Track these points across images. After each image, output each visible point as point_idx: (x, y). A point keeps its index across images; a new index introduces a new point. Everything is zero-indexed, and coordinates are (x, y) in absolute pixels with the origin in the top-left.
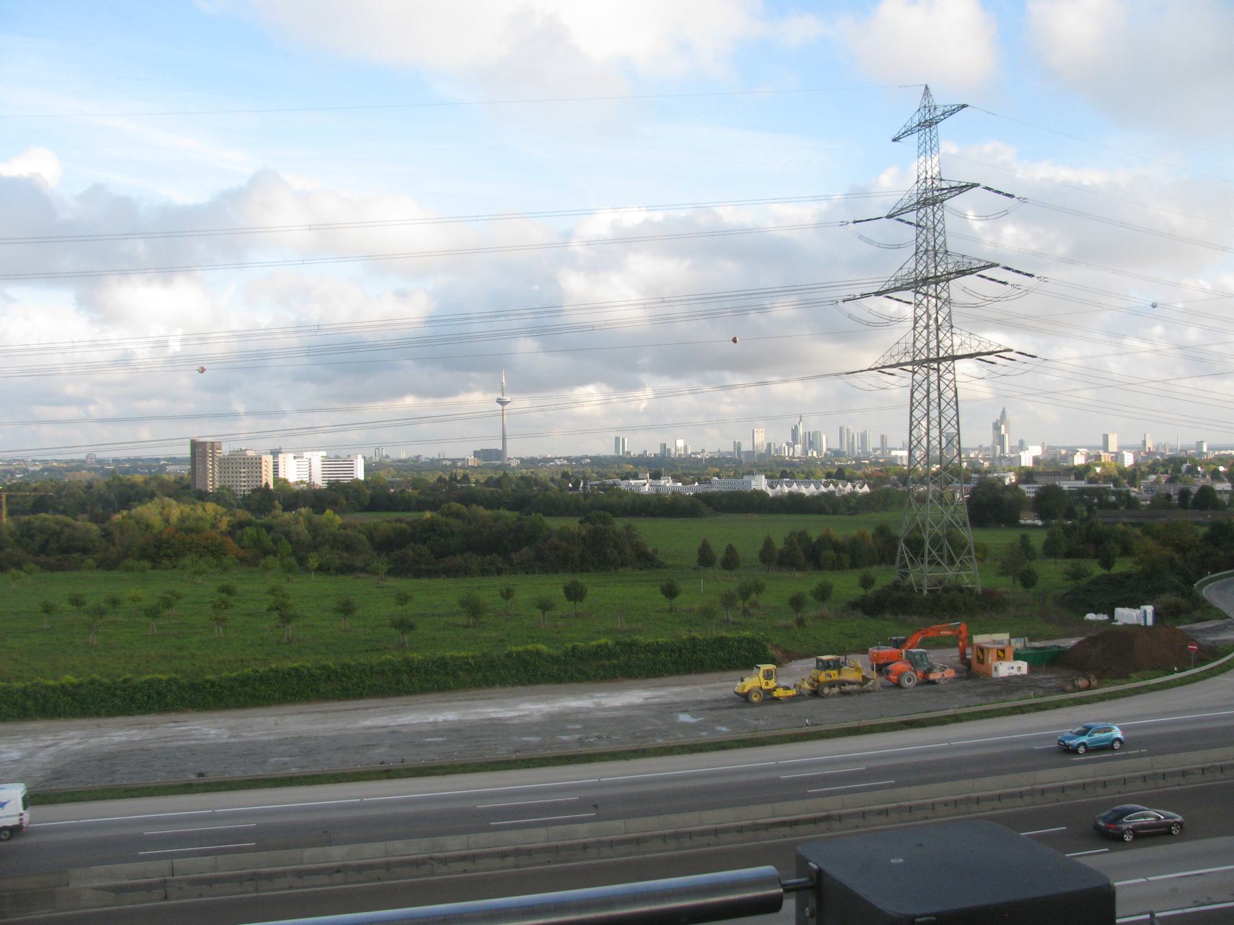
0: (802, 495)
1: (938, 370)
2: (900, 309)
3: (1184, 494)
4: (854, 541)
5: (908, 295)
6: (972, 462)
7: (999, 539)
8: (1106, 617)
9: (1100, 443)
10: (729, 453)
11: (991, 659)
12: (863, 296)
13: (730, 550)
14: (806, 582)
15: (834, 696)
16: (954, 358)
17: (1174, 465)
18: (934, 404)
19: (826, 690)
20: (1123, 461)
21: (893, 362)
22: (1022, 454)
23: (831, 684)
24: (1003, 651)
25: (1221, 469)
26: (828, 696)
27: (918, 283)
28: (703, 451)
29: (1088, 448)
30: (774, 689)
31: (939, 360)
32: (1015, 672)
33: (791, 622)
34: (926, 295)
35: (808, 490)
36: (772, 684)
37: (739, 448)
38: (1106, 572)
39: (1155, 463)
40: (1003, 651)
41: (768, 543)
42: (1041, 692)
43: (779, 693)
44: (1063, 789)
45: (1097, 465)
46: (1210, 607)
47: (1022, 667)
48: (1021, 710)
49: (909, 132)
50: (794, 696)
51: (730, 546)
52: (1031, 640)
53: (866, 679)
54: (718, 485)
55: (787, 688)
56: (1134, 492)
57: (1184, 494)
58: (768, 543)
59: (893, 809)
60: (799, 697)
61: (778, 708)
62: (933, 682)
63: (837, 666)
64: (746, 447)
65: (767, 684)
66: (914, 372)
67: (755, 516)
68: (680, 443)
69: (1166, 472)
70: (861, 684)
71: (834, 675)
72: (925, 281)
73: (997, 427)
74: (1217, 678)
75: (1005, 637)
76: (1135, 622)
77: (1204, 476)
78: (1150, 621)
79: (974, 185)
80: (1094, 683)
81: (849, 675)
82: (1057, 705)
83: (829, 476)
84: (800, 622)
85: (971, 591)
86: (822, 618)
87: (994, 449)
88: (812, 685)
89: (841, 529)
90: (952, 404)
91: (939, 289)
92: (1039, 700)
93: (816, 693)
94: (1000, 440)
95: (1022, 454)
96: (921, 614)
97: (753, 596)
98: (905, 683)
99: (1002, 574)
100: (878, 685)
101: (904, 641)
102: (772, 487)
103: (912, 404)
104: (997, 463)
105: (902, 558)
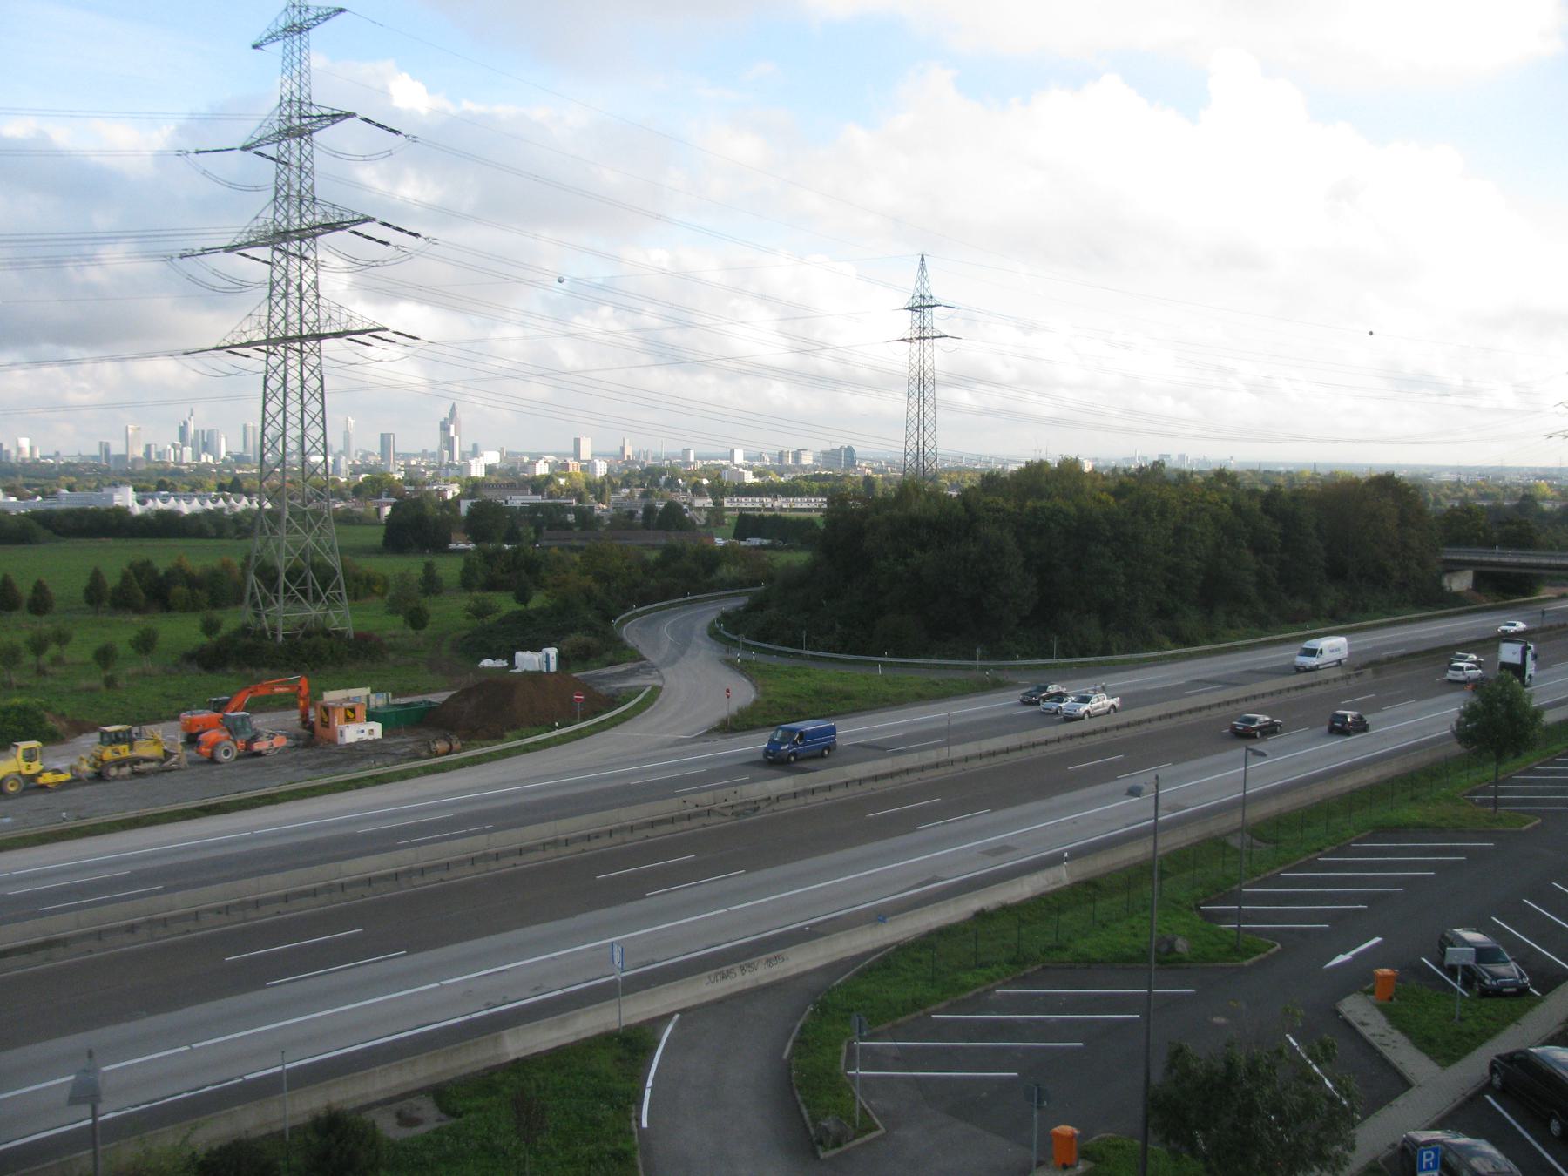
0: (179, 512)
1: (301, 352)
2: (254, 268)
3: (649, 510)
4: (215, 574)
5: (264, 253)
6: (408, 469)
7: (411, 566)
8: (505, 663)
9: (572, 450)
10: (94, 457)
11: (338, 722)
12: (205, 251)
13: (40, 588)
14: (122, 630)
15: (124, 778)
16: (320, 337)
17: (651, 476)
18: (294, 396)
19: (113, 772)
20: (594, 472)
21: (244, 340)
22: (473, 462)
23: (120, 763)
24: (353, 710)
25: (705, 482)
26: (115, 778)
27: (278, 238)
28: (57, 454)
29: (555, 454)
30: (39, 774)
31: (302, 338)
32: (366, 736)
33: (98, 682)
34: (286, 253)
35: (186, 507)
36: (36, 767)
37: (107, 451)
38: (520, 607)
39: (631, 474)
40: (353, 710)
41: (96, 578)
42: (390, 760)
43: (47, 778)
44: (370, 881)
45: (561, 476)
46: (626, 648)
47: (377, 729)
48: (357, 784)
49: (273, 37)
50: (68, 782)
51: (39, 583)
52: (394, 696)
53: (168, 755)
54: (66, 500)
55: (58, 772)
56: (601, 508)
57: (649, 510)
58: (96, 578)
59: (142, 923)
60: (76, 781)
61: (41, 799)
62: (259, 754)
63: (128, 739)
64: (117, 448)
65: (29, 768)
66: (268, 352)
67: (111, 542)
68: (25, 443)
69: (642, 485)
70: (161, 761)
71: (124, 751)
72: (285, 235)
73: (444, 427)
74: (607, 733)
75: (366, 691)
76: (537, 668)
77: (685, 490)
78: (553, 667)
79: (348, 115)
80: (457, 746)
81: (144, 749)
82: (404, 776)
83: (221, 487)
84: (110, 683)
85: (340, 635)
86: (144, 674)
87: (442, 456)
88: (94, 766)
89: (198, 558)
90: (317, 396)
91: (304, 246)
92: (381, 771)
93: (99, 776)
94: (449, 444)
95: (473, 462)
96: (273, 666)
97: (53, 649)
98: (221, 756)
99: (391, 612)
100: (184, 761)
101: (227, 702)
102: (142, 502)
103: (265, 395)
104: (442, 472)
105: (253, 595)
